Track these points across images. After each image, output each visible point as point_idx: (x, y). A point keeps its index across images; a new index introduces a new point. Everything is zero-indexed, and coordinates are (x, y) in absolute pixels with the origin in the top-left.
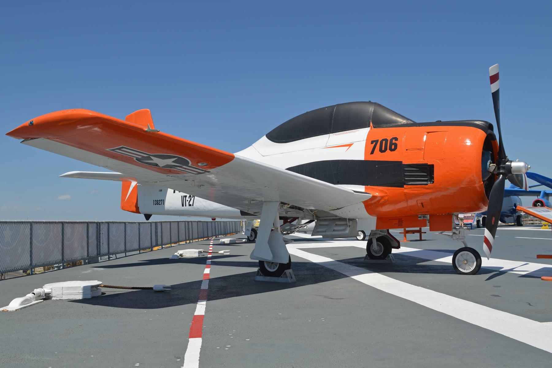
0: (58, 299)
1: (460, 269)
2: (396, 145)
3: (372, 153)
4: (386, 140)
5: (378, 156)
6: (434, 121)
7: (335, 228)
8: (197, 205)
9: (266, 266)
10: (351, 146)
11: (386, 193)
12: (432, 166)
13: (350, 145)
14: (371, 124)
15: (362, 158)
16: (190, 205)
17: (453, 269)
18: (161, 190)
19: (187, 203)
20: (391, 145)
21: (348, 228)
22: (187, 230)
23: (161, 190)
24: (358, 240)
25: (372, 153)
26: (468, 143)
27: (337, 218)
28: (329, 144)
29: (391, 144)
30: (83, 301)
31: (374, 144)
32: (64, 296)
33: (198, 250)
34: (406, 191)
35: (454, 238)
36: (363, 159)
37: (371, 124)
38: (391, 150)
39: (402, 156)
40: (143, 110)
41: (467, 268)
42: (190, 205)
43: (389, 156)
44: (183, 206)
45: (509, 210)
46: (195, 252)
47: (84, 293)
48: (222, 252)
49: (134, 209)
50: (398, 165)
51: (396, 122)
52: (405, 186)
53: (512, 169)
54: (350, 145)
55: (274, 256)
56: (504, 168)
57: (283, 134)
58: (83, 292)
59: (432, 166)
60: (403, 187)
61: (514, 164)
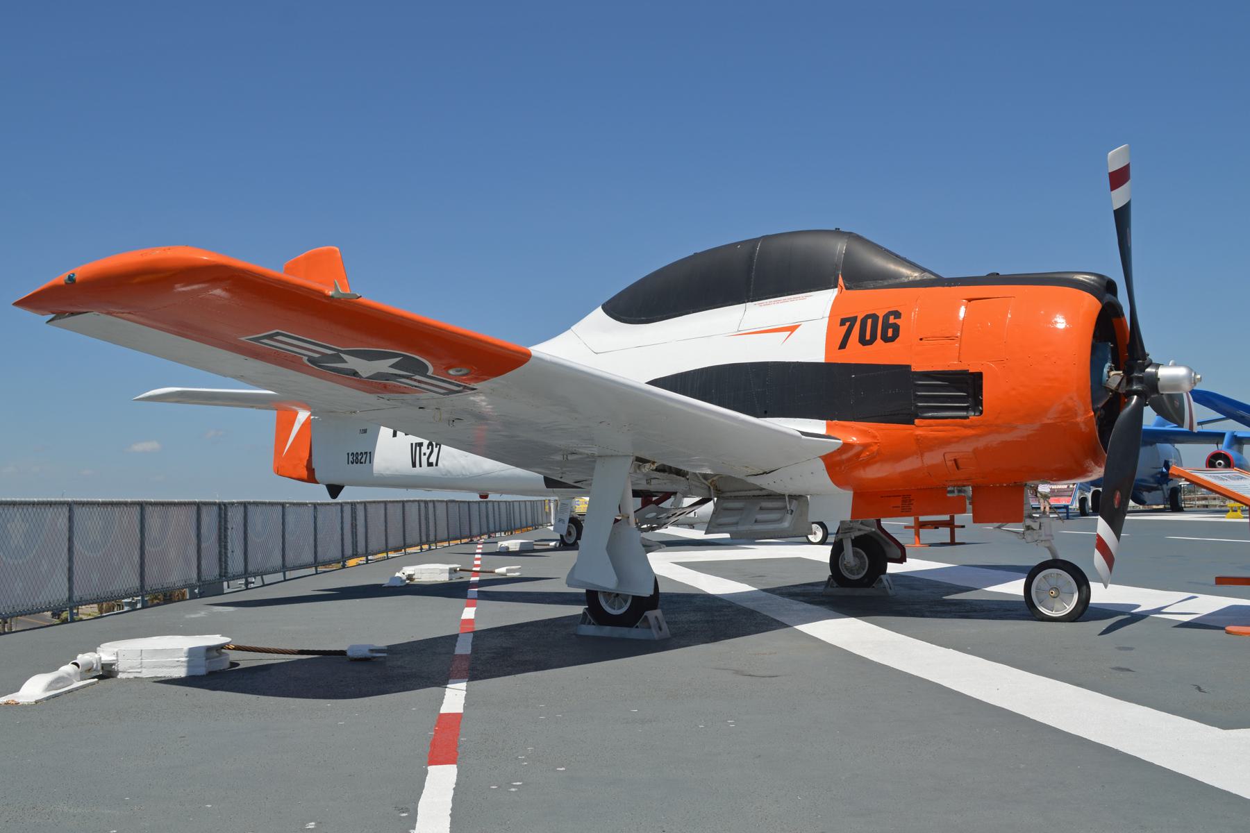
0: (131, 676)
1: (1042, 609)
2: (896, 329)
3: (843, 346)
4: (874, 317)
5: (857, 354)
6: (983, 273)
7: (759, 517)
8: (446, 463)
9: (603, 603)
10: (794, 330)
11: (875, 437)
12: (979, 376)
13: (792, 329)
14: (841, 281)
15: (820, 358)
16: (430, 464)
17: (1026, 609)
18: (365, 431)
19: (424, 459)
20: (885, 328)
21: (789, 517)
22: (423, 522)
23: (365, 431)
24: (810, 543)
25: (843, 346)
26: (1061, 323)
27: (764, 493)
28: (746, 327)
29: (886, 326)
30: (189, 681)
31: (846, 327)
32: (144, 670)
33: (447, 567)
34: (918, 432)
35: (1029, 538)
36: (823, 360)
37: (841, 281)
38: (886, 339)
39: (911, 352)
40: (325, 248)
41: (1057, 606)
42: (430, 464)
43: (880, 354)
44: (414, 465)
45: (1153, 476)
46: (442, 571)
47: (190, 664)
48: (502, 570)
49: (305, 474)
50: (901, 373)
51: (896, 276)
52: (916, 421)
53: (1160, 384)
54: (792, 329)
55: (621, 579)
56: (1140, 380)
57: (641, 304)
58: (188, 662)
59: (979, 376)
60: (913, 423)
61: (1163, 372)
